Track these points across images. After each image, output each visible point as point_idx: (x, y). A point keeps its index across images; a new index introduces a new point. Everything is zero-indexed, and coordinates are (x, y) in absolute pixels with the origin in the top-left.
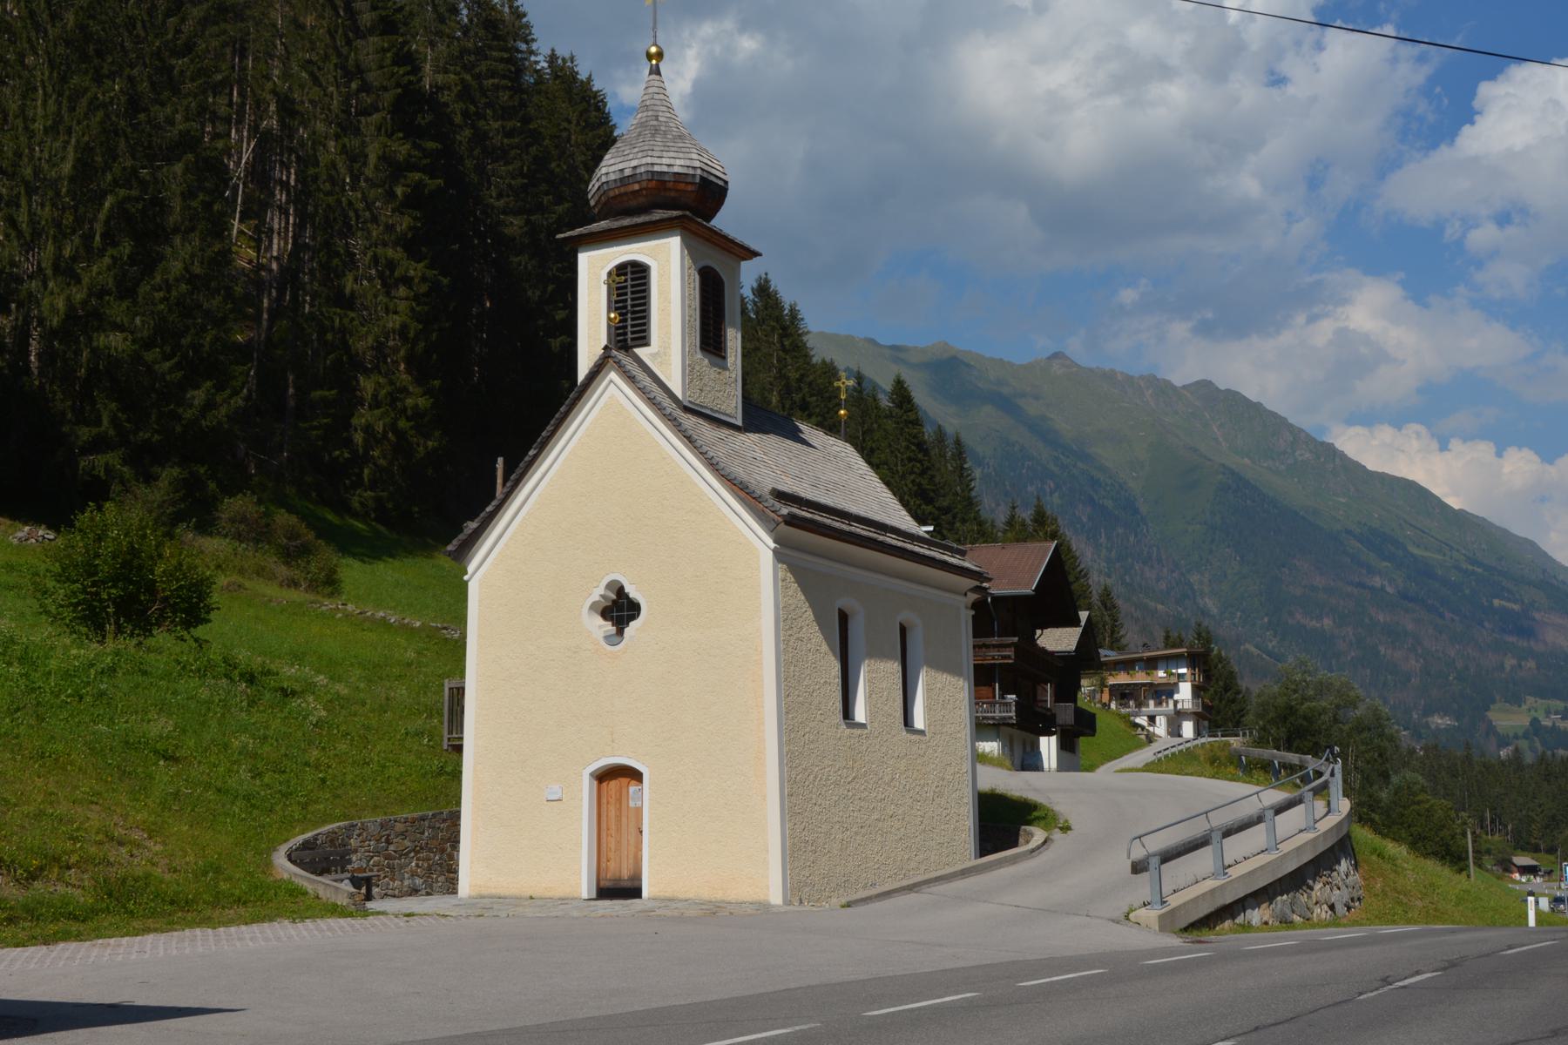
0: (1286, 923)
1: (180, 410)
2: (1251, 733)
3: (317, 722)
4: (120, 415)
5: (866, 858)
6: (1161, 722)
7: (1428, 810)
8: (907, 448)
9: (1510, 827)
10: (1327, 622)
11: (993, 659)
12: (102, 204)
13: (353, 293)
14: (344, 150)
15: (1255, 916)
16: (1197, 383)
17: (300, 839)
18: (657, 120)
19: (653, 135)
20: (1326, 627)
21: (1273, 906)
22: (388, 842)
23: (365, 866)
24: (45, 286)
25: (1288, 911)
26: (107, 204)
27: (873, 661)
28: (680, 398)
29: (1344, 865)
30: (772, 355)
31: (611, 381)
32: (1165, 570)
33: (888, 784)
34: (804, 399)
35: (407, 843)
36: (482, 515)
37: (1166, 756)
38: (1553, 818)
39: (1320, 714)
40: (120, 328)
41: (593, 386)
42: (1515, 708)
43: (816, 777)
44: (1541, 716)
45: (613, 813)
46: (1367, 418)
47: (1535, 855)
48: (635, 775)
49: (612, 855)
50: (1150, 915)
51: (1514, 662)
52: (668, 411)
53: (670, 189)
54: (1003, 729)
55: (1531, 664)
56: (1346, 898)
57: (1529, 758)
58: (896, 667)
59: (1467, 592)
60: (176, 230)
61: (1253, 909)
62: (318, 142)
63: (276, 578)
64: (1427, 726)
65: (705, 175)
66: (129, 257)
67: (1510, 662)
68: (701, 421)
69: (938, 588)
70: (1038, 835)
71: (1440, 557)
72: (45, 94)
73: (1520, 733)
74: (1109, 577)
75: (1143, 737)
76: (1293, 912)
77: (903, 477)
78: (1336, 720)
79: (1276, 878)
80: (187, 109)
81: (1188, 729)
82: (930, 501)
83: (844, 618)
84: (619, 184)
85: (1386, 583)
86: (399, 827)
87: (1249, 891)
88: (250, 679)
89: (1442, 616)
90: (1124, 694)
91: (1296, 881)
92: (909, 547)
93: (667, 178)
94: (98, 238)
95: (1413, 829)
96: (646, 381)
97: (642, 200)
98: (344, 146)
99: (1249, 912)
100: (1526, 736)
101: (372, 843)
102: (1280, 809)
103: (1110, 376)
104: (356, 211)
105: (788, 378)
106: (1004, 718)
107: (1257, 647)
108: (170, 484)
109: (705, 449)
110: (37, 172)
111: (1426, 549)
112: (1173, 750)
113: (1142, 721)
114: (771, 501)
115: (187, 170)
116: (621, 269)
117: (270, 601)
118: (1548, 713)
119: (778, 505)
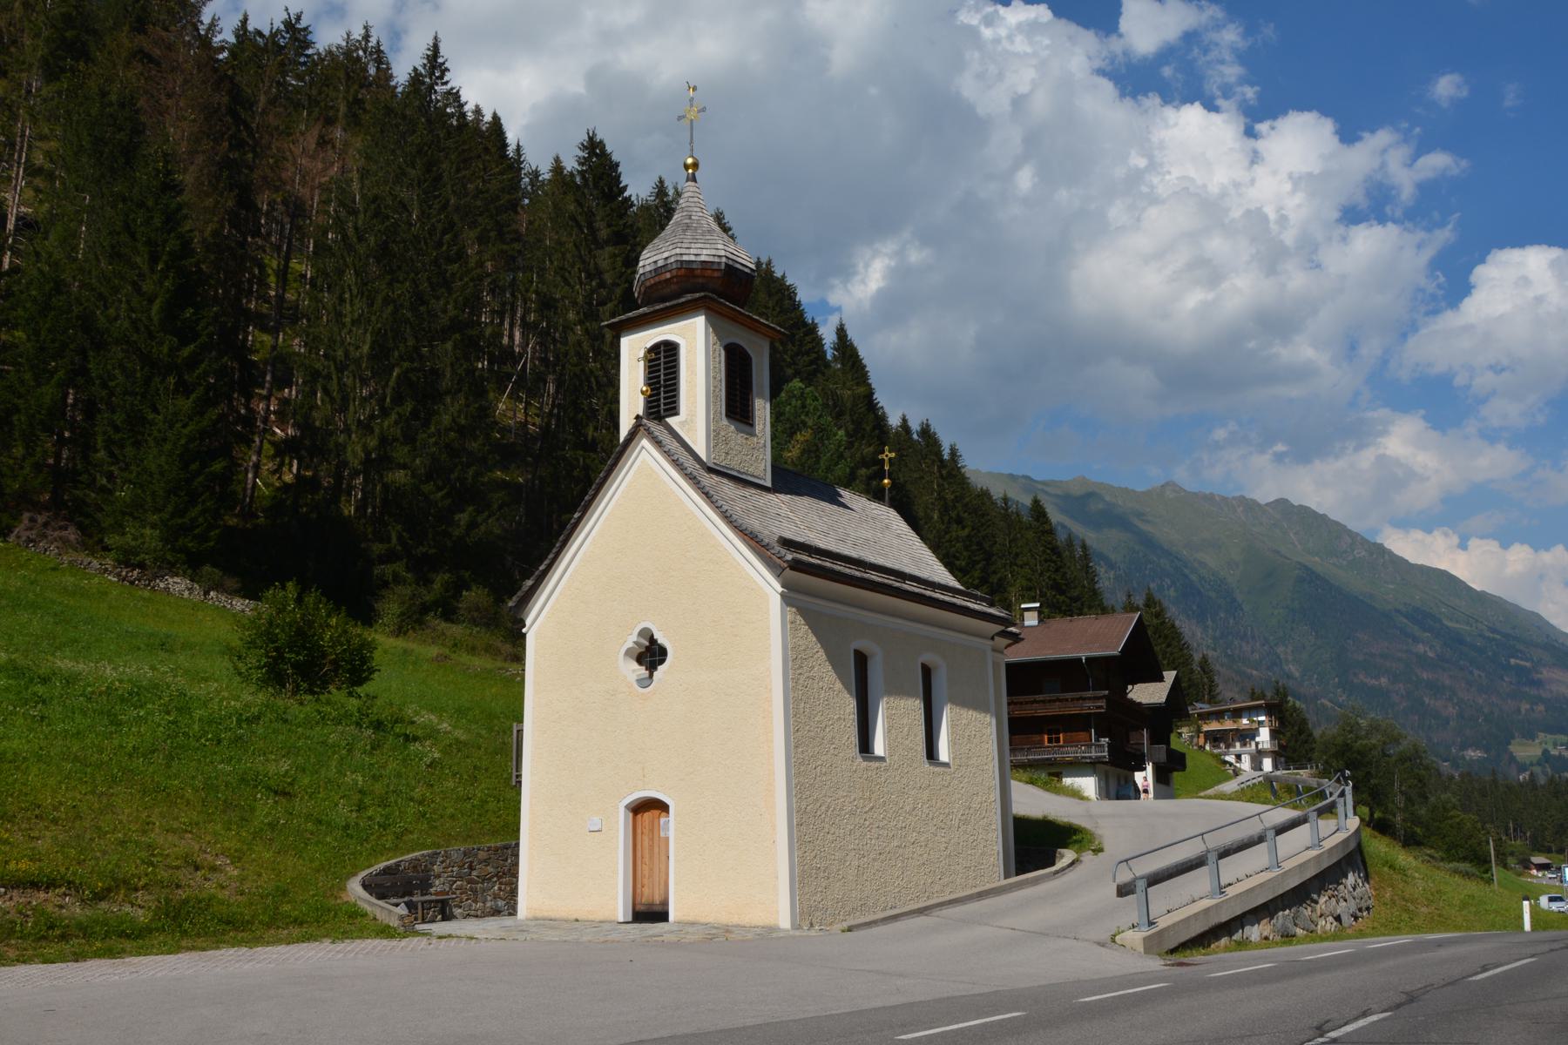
0: (1287, 936)
1: (450, 530)
2: (1317, 767)
3: (432, 763)
4: (404, 534)
5: (885, 882)
6: (1246, 759)
7: (1458, 824)
8: (1044, 552)
9: (1528, 834)
10: (1384, 680)
11: (1089, 709)
12: (391, 374)
13: (594, 439)
14: (587, 332)
15: (1254, 932)
16: (1277, 501)
17: (382, 865)
18: (690, 218)
19: (684, 231)
20: (1383, 685)
21: (1274, 921)
22: (471, 868)
23: (447, 889)
24: (350, 437)
25: (1290, 925)
26: (395, 374)
27: (892, 699)
28: (705, 460)
29: (1351, 879)
30: (932, 482)
31: (643, 447)
32: (1258, 644)
33: (909, 813)
34: (958, 515)
35: (490, 869)
36: (537, 573)
37: (1249, 786)
38: (1562, 825)
39: (1371, 749)
40: (404, 467)
41: (627, 452)
42: (1530, 742)
43: (829, 807)
44: (1550, 748)
45: (646, 843)
46: (1404, 523)
47: (1549, 855)
48: (662, 807)
49: (646, 881)
50: (1135, 938)
51: (1528, 706)
52: (689, 470)
53: (698, 277)
54: (1098, 765)
55: (1541, 708)
56: (1353, 909)
57: (1542, 780)
58: (917, 705)
59: (1490, 654)
60: (448, 392)
61: (1253, 925)
62: (568, 328)
63: (501, 654)
64: (1463, 757)
65: (731, 263)
66: (410, 413)
67: (1525, 707)
68: (725, 481)
69: (965, 633)
70: (1067, 855)
71: (1468, 628)
72: (351, 295)
73: (1535, 762)
74: (1215, 650)
75: (1231, 772)
76: (1296, 925)
77: (1041, 574)
78: (1385, 755)
79: (1276, 895)
80: (456, 302)
81: (1267, 764)
82: (1062, 593)
83: (861, 660)
84: (653, 274)
85: (1427, 649)
86: (482, 855)
87: (1247, 909)
88: (378, 725)
89: (1471, 673)
90: (1216, 738)
91: (1300, 895)
92: (928, 593)
93: (694, 266)
94: (388, 400)
95: (1447, 839)
96: (673, 445)
97: (674, 287)
98: (587, 329)
99: (1247, 929)
100: (1539, 764)
101: (455, 869)
102: (1281, 830)
103: (1210, 498)
104: (596, 378)
105: (945, 499)
106: (1100, 757)
107: (1331, 701)
108: (442, 585)
109: (720, 503)
110: (347, 354)
111: (1457, 622)
112: (1254, 781)
113: (1231, 759)
114: (778, 548)
115: (455, 347)
116: (654, 349)
117: (468, 668)
118: (1555, 745)
119: (783, 551)
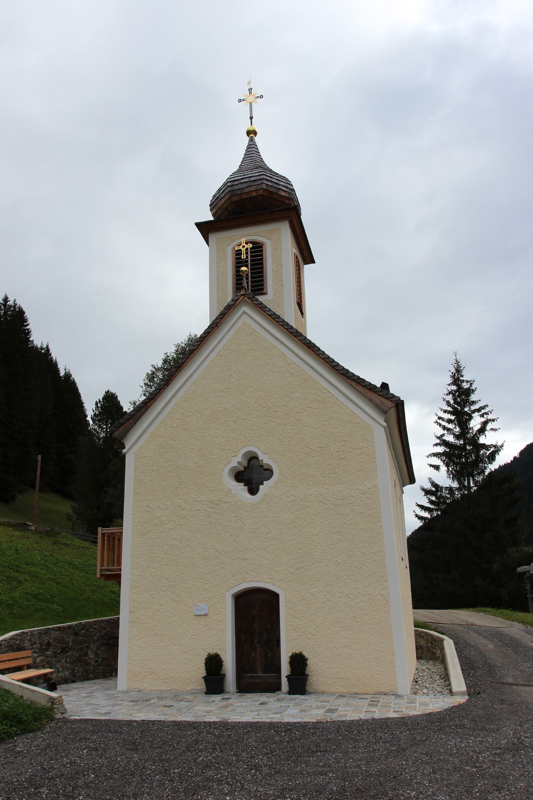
31: (244, 312)
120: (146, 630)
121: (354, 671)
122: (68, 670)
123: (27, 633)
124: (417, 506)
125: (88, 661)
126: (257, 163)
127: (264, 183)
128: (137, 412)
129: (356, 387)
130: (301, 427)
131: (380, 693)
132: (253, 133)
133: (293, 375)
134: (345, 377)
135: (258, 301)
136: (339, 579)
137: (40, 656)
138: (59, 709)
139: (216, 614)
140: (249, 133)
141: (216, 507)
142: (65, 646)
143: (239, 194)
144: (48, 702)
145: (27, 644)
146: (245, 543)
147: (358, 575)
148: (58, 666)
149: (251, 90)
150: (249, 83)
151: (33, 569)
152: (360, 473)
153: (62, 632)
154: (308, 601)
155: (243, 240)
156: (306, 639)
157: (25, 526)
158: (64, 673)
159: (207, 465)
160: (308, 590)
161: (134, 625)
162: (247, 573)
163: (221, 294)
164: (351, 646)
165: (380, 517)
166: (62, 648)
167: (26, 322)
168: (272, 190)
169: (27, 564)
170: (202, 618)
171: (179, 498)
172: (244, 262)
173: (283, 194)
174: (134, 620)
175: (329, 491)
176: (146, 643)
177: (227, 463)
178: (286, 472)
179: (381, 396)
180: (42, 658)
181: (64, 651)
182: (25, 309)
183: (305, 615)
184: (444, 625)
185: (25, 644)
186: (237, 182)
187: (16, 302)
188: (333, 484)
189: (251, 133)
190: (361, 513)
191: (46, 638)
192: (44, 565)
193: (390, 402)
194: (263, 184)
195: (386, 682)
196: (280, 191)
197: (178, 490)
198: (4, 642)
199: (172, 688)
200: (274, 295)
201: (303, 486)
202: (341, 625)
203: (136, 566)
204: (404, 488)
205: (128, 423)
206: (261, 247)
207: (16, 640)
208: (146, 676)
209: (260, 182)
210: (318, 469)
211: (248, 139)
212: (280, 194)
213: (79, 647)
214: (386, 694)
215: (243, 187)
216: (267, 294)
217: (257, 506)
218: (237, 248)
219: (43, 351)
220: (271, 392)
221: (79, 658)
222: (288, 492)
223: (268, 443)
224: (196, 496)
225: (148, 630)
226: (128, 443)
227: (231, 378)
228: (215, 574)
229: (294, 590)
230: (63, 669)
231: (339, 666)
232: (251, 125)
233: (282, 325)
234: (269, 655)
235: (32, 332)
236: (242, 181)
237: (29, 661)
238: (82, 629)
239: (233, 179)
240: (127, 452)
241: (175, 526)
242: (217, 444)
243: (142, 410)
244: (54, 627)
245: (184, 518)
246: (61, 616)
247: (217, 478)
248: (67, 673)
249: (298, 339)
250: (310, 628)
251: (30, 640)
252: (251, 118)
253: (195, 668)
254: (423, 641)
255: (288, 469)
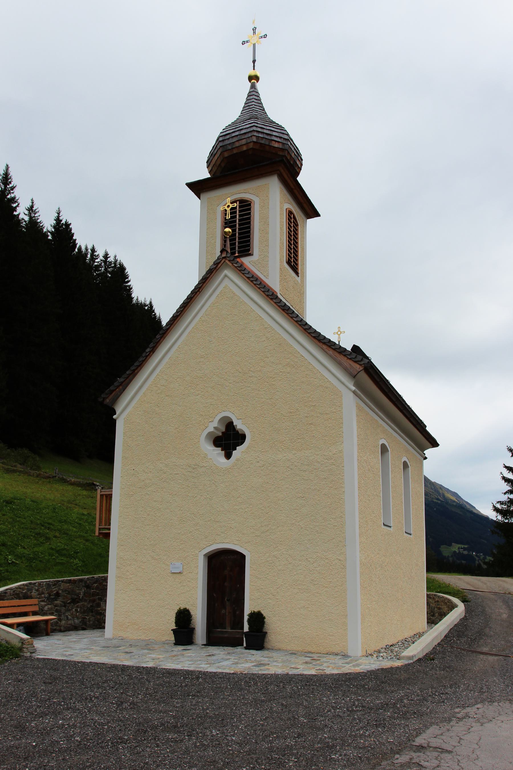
31: (226, 276)
120: (130, 585)
121: (309, 631)
122: (78, 618)
123: (35, 583)
124: (505, 467)
125: (101, 611)
126: (253, 113)
127: (254, 136)
128: (125, 379)
129: (327, 350)
130: (273, 392)
131: (331, 653)
132: (254, 78)
133: (269, 339)
134: (317, 340)
135: (238, 263)
136: (300, 543)
137: (48, 604)
138: (28, 649)
139: (189, 572)
140: (250, 78)
141: (193, 471)
142: (76, 597)
143: (231, 149)
144: (19, 642)
145: (34, 593)
146: (218, 506)
147: (319, 539)
148: (67, 614)
149: (255, 30)
150: (253, 23)
151: (65, 527)
152: (327, 439)
153: (73, 584)
154: (271, 563)
155: (229, 200)
156: (268, 599)
157: (93, 486)
158: (74, 621)
159: (187, 430)
160: (272, 553)
161: (119, 580)
162: (217, 535)
163: (210, 257)
164: (308, 608)
165: (343, 483)
166: (72, 599)
167: (127, 278)
168: (263, 142)
169: (60, 522)
170: (177, 575)
171: (161, 462)
172: (228, 223)
173: (276, 145)
174: (120, 575)
175: (296, 457)
176: (130, 597)
177: (204, 429)
178: (257, 437)
179: (350, 359)
180: (50, 606)
181: (74, 601)
182: (125, 265)
183: (268, 577)
184: (481, 593)
185: (32, 593)
186: (228, 137)
187: (116, 258)
188: (300, 449)
189: (253, 78)
190: (325, 478)
191: (54, 589)
192: (77, 523)
193: (359, 365)
194: (253, 137)
195: (337, 643)
196: (273, 142)
197: (161, 454)
198: (9, 590)
199: (150, 638)
200: (260, 256)
201: (273, 451)
202: (299, 588)
203: (123, 526)
204: (424, 452)
205: (118, 390)
206: (250, 205)
207: (23, 589)
208: (129, 626)
209: (250, 135)
210: (287, 435)
211: (249, 84)
212: (273, 145)
213: (91, 599)
214: (336, 655)
215: (233, 141)
216: (253, 255)
217: (229, 471)
218: (234, 205)
219: (146, 308)
220: (247, 357)
221: (91, 608)
222: (259, 457)
223: (242, 408)
224: (176, 460)
225: (131, 585)
226: (119, 409)
227: (211, 344)
228: (190, 535)
229: (259, 552)
230: (73, 618)
231: (295, 626)
232: (254, 69)
233: (259, 288)
234: (237, 613)
235: (133, 289)
236: (233, 135)
237: (36, 609)
238: (95, 583)
239: (224, 134)
240: (118, 418)
241: (157, 489)
242: (196, 410)
243: (129, 378)
244: (64, 580)
245: (165, 481)
246: (79, 570)
247: (195, 443)
248: (77, 621)
249: (273, 301)
250: (271, 589)
251: (37, 590)
252: (254, 61)
253: (169, 621)
254: (446, 607)
255: (260, 434)
